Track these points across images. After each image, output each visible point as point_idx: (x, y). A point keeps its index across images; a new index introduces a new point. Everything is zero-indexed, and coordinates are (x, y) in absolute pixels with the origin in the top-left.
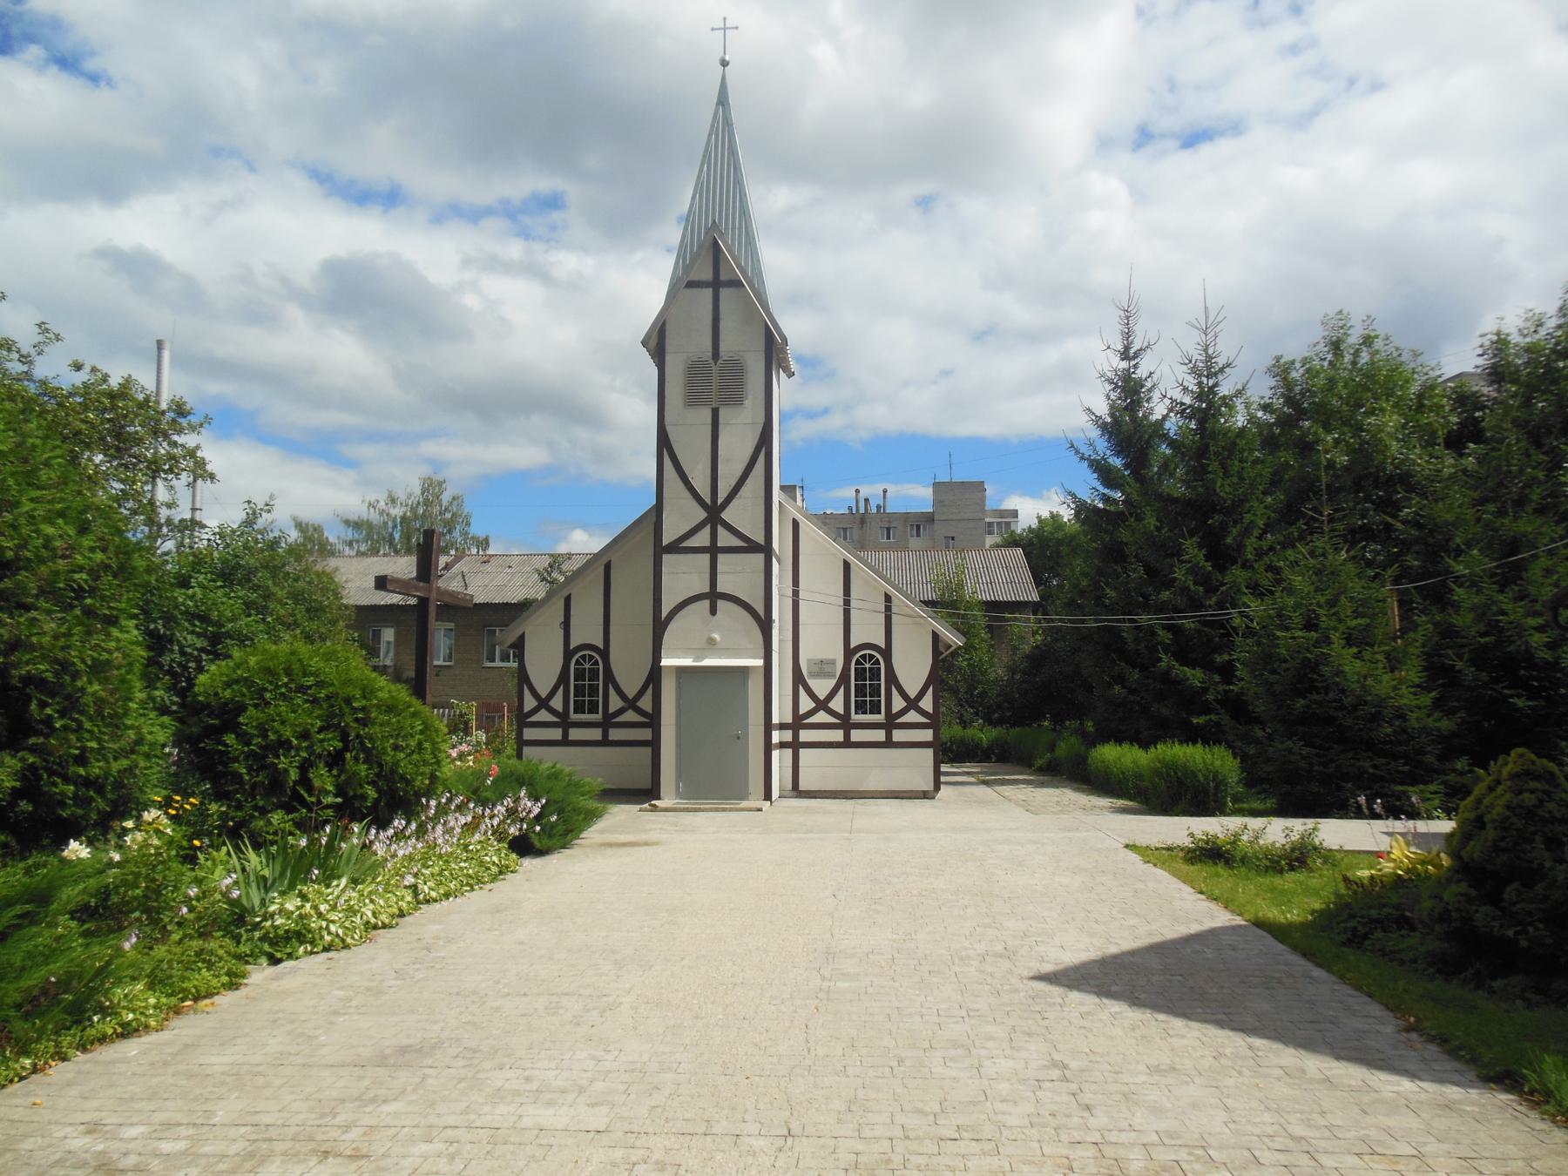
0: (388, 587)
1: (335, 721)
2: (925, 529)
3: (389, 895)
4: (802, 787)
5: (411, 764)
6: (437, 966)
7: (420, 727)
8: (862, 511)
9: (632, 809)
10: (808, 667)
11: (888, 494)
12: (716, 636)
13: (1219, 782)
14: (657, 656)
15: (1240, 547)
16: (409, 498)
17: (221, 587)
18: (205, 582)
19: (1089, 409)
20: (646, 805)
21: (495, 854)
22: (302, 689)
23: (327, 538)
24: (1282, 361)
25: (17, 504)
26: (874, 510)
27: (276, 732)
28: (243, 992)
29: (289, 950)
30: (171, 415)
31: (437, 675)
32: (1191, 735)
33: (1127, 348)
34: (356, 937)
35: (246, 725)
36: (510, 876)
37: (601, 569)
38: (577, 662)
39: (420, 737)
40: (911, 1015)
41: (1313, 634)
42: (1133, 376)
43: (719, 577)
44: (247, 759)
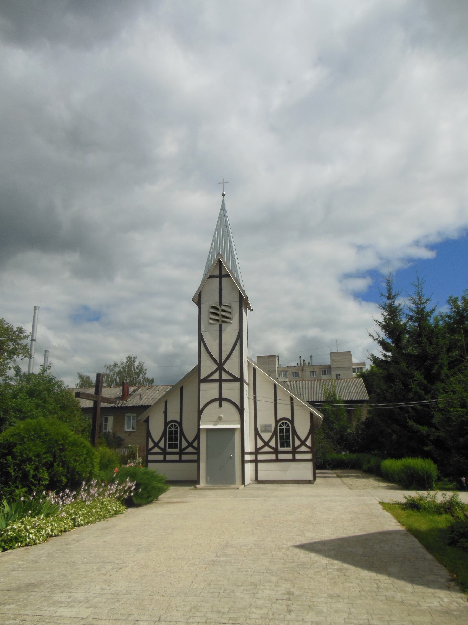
0: (80, 396)
1: (51, 450)
2: (328, 371)
3: (61, 522)
4: (259, 479)
5: (81, 467)
6: (66, 551)
7: (86, 452)
8: (302, 365)
9: (187, 488)
10: (261, 428)
11: (312, 358)
12: (222, 416)
13: (429, 476)
14: (199, 425)
15: (439, 374)
16: (122, 364)
17: (28, 398)
18: (23, 397)
19: (376, 320)
20: (193, 487)
21: (114, 506)
22: (39, 437)
23: (91, 381)
24: (453, 298)
26: (307, 364)
27: (27, 455)
29: (11, 545)
30: (17, 333)
32: (413, 453)
33: (390, 295)
34: (41, 540)
35: (16, 452)
36: (119, 516)
37: (179, 390)
38: (170, 428)
39: (85, 456)
40: (242, 572)
41: (464, 409)
42: (393, 306)
43: (223, 391)
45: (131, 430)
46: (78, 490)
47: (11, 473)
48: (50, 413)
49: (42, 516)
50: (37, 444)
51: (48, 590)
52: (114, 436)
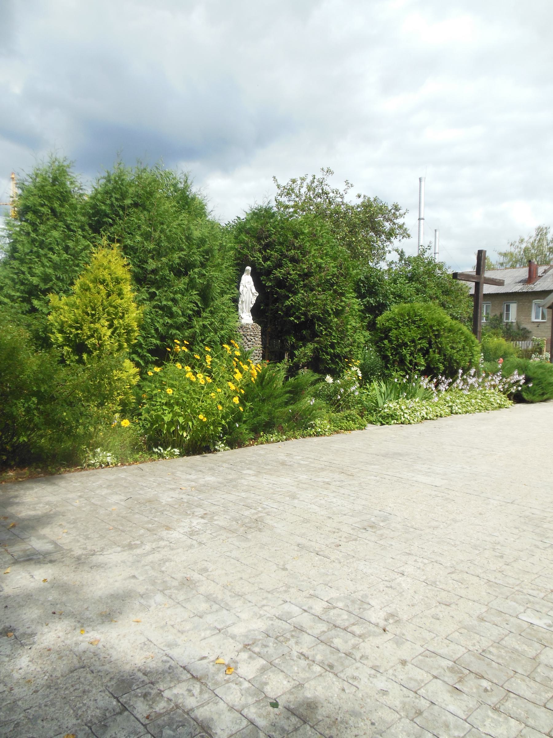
18: (402, 281)
21: (501, 398)
22: (414, 322)
25: (310, 252)
28: (364, 431)
29: (387, 421)
30: (393, 211)
31: (538, 326)
44: (391, 350)
45: (540, 320)
46: (454, 378)
47: (388, 356)
48: (431, 298)
49: (417, 400)
50: (412, 328)
51: (412, 460)
52: (518, 328)
